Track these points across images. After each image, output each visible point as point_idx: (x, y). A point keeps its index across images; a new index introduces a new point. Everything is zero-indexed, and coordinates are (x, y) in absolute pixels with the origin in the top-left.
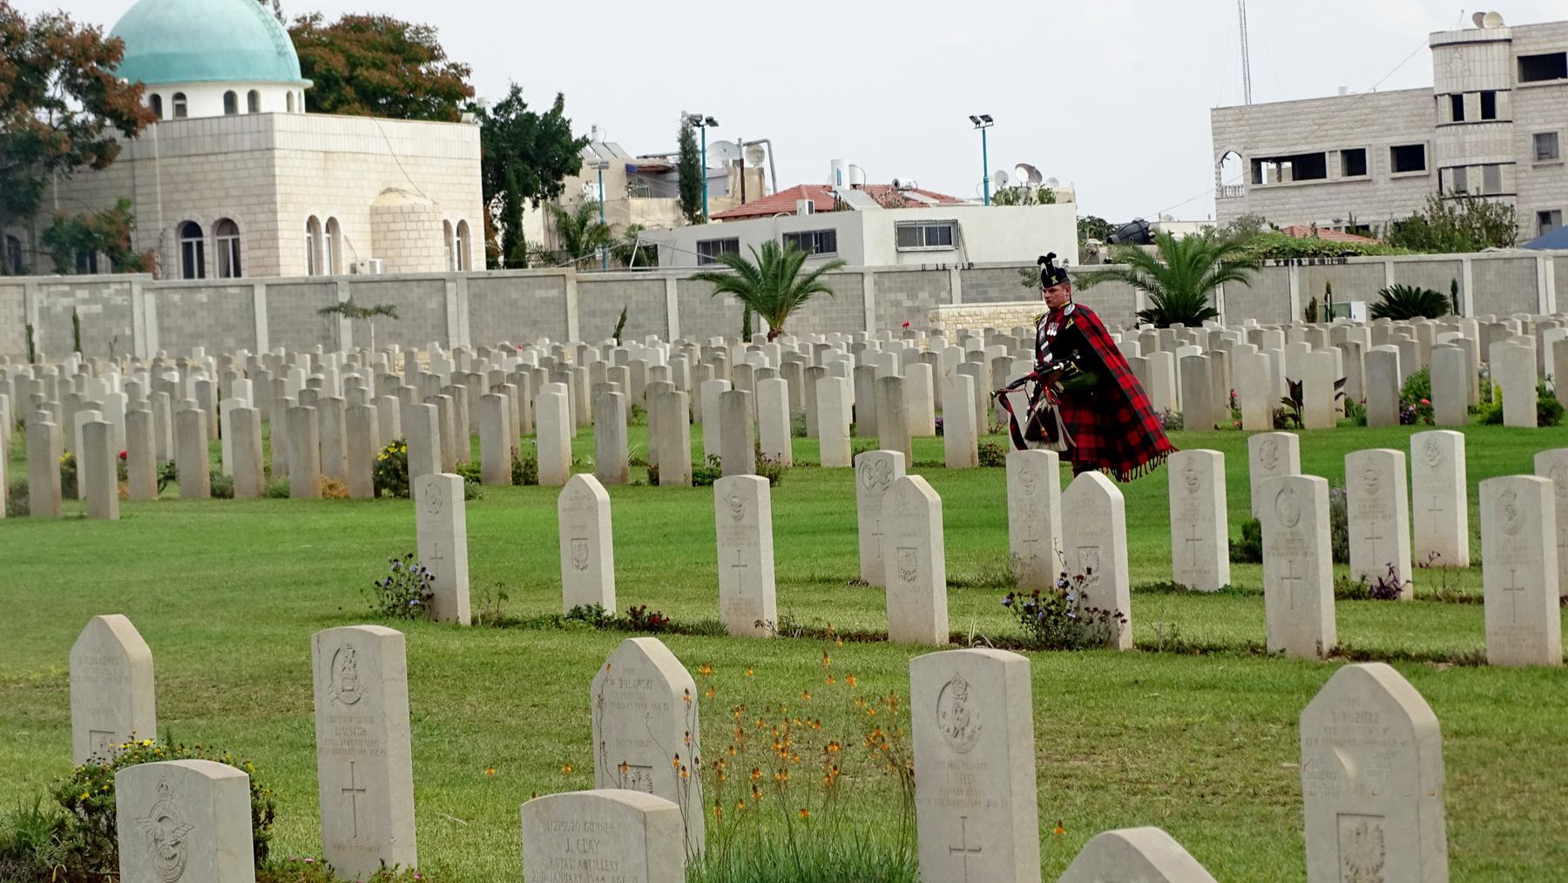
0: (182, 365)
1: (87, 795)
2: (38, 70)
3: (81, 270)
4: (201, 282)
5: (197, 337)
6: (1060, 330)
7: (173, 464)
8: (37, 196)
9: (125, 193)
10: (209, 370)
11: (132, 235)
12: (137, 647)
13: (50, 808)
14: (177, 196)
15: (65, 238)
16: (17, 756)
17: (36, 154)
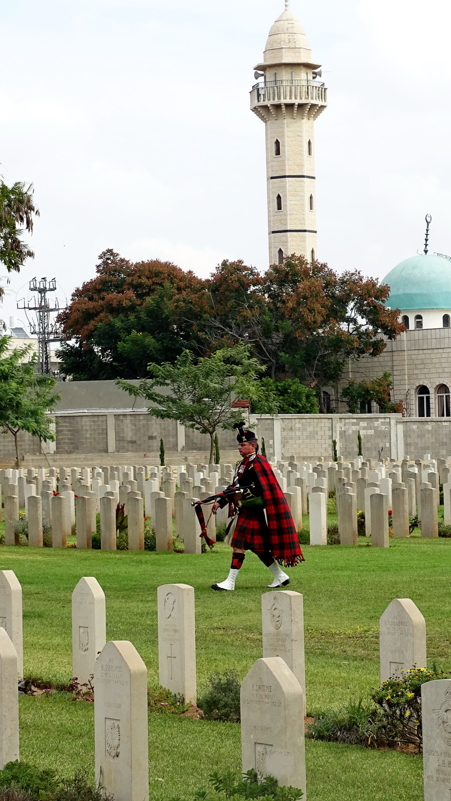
0: (418, 464)
1: (389, 697)
2: (342, 302)
3: (363, 411)
4: (429, 419)
5: (425, 449)
6: (246, 470)
7: (416, 518)
8: (340, 370)
9: (388, 369)
10: (434, 467)
11: (391, 392)
12: (417, 616)
13: (370, 704)
14: (416, 372)
15: (355, 393)
16: (343, 675)
17: (340, 347)
